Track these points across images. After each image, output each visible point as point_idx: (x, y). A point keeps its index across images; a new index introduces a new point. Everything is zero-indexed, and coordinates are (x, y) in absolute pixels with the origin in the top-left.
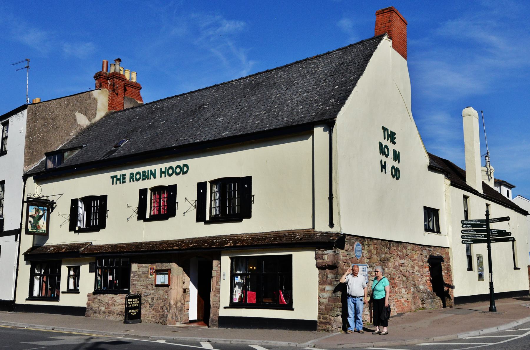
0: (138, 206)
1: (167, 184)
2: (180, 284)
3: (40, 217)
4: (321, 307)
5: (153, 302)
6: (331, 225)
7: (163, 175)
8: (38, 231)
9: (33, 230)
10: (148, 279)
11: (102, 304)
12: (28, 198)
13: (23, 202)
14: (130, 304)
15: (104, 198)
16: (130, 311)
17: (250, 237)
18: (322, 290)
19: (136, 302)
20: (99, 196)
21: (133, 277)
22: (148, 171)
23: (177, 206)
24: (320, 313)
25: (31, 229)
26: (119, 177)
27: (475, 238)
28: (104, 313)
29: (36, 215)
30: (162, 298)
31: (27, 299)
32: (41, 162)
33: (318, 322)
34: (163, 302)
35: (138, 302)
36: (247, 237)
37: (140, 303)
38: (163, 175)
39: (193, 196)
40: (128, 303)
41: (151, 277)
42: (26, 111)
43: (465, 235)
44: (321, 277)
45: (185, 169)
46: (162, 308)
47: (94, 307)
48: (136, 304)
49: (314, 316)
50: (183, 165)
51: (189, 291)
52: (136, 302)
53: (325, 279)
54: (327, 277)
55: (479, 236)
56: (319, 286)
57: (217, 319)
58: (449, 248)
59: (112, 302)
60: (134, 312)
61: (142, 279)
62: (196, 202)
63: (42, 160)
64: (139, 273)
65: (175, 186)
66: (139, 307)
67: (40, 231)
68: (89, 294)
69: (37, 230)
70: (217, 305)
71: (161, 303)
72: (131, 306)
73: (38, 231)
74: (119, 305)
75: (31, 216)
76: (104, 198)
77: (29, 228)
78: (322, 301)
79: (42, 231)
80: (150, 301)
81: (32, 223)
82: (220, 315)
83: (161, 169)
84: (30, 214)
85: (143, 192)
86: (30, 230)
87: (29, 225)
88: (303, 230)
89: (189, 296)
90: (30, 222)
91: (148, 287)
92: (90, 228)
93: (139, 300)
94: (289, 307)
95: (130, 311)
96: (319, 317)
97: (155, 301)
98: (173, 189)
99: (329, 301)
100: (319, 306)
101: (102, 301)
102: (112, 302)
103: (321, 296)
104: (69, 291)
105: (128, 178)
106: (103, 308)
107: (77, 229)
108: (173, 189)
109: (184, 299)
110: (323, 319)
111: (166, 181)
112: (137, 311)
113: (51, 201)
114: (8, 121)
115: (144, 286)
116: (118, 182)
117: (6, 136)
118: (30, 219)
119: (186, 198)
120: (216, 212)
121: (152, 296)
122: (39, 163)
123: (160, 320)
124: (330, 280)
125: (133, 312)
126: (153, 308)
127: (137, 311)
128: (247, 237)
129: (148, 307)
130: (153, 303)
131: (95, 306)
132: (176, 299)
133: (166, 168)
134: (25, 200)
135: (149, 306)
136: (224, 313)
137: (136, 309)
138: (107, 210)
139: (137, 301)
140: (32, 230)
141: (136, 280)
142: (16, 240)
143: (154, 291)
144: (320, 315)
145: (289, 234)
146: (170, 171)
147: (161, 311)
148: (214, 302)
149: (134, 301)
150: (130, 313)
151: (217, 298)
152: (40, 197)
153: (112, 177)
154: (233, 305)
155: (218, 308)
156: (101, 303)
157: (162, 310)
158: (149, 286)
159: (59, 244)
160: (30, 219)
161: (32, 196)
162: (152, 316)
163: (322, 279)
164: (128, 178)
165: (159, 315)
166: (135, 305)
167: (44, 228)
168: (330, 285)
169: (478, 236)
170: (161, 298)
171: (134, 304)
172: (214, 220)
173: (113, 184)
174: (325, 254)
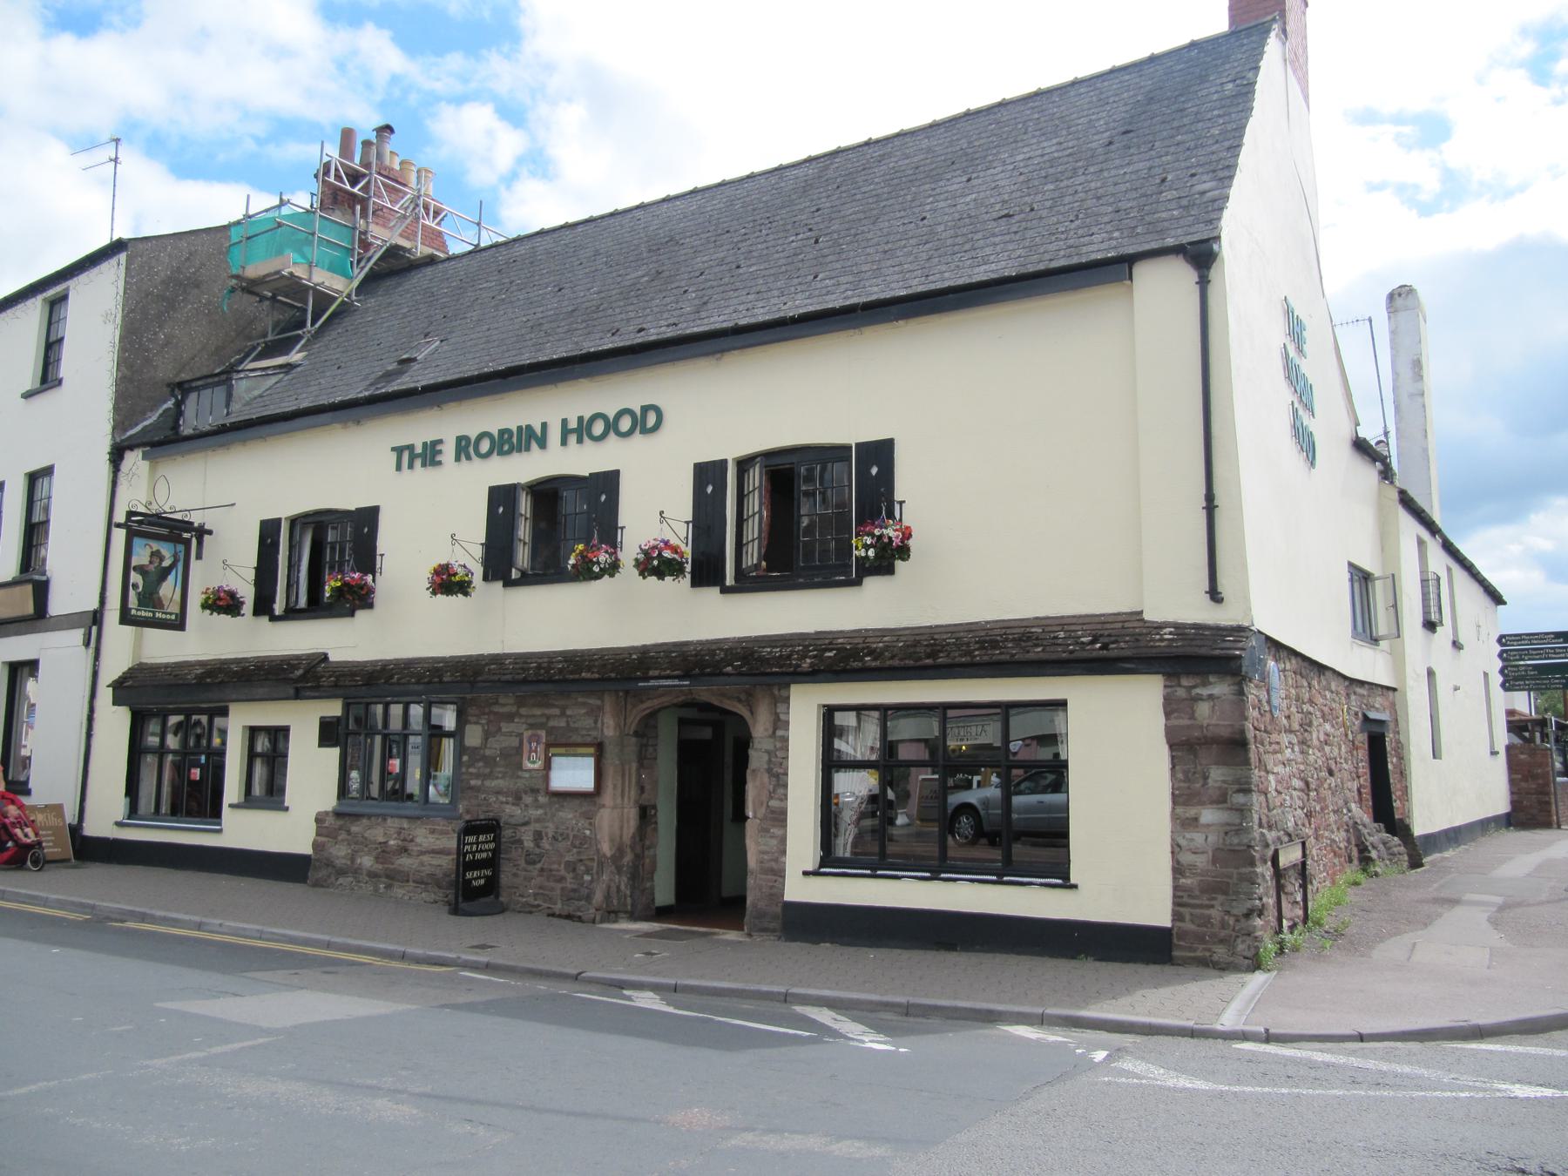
0: (484, 541)
1: (584, 471)
2: (629, 792)
3: (164, 573)
4: (1183, 881)
5: (539, 847)
6: (1215, 595)
7: (573, 439)
8: (157, 615)
9: (143, 614)
10: (520, 773)
11: (366, 849)
12: (130, 514)
13: (110, 524)
14: (471, 852)
15: (369, 517)
16: (469, 875)
17: (898, 641)
18: (1183, 823)
19: (486, 846)
20: (353, 509)
21: (469, 767)
22: (520, 428)
23: (619, 540)
24: (1178, 903)
25: (137, 610)
26: (419, 450)
27: (1545, 659)
28: (373, 875)
29: (152, 568)
30: (571, 838)
31: (119, 824)
32: (164, 411)
33: (1174, 932)
34: (575, 847)
35: (492, 846)
36: (886, 639)
37: (496, 852)
38: (573, 439)
39: (682, 508)
40: (466, 847)
41: (530, 766)
42: (123, 257)
43: (1511, 650)
44: (1180, 776)
45: (651, 419)
46: (571, 867)
47: (338, 858)
48: (486, 851)
49: (1155, 910)
50: (642, 407)
51: (655, 814)
52: (486, 846)
53: (1198, 785)
54: (1206, 778)
55: (1559, 653)
56: (1173, 809)
57: (779, 910)
58: (1394, 690)
59: (400, 843)
60: (480, 878)
61: (500, 772)
62: (691, 525)
63: (165, 406)
64: (488, 752)
65: (615, 475)
66: (493, 863)
67: (164, 616)
68: (319, 814)
69: (154, 613)
70: (773, 865)
71: (568, 852)
72: (474, 857)
73: (157, 615)
74: (422, 853)
75: (135, 569)
76: (369, 517)
77: (130, 606)
78: (1187, 858)
79: (168, 617)
80: (528, 843)
81: (140, 589)
82: (787, 898)
83: (565, 422)
84: (134, 563)
85: (501, 497)
86: (133, 612)
87: (132, 594)
88: (1114, 614)
89: (655, 830)
90: (135, 586)
91: (520, 799)
92: (316, 608)
93: (494, 841)
94: (1058, 872)
95: (469, 875)
96: (1177, 916)
97: (545, 844)
98: (608, 482)
99: (1214, 862)
100: (1175, 879)
101: (366, 839)
102: (400, 843)
103: (1183, 842)
104: (249, 801)
105: (449, 450)
106: (367, 861)
107: (515, 574)
108: (608, 482)
109: (641, 840)
110: (1192, 921)
111: (581, 461)
112: (488, 873)
113: (196, 525)
114: (67, 289)
115: (506, 794)
116: (418, 462)
117: (59, 337)
118: (135, 577)
119: (662, 513)
120: (752, 556)
121: (538, 826)
122: (157, 415)
123: (566, 907)
124: (1220, 788)
125: (477, 878)
126: (539, 866)
127: (488, 873)
128: (886, 639)
129: (523, 861)
130: (537, 851)
131: (339, 852)
132: (618, 839)
133: (580, 419)
134: (120, 517)
135: (526, 861)
136: (800, 889)
137: (486, 868)
138: (378, 553)
139: (490, 842)
140: (139, 613)
141: (477, 776)
142: (87, 644)
143: (540, 812)
144: (1182, 909)
145: (1047, 629)
146: (598, 428)
147: (569, 876)
148: (762, 856)
149: (483, 842)
150: (470, 881)
151: (774, 842)
152: (165, 513)
153: (399, 451)
154: (829, 861)
155: (780, 874)
156: (360, 843)
157: (571, 875)
158: (524, 796)
159: (223, 657)
160: (135, 577)
161: (142, 509)
162: (537, 891)
163: (1186, 785)
164: (449, 450)
165: (562, 889)
166: (484, 855)
167: (175, 608)
168: (1220, 806)
169: (1555, 653)
170: (568, 835)
171: (482, 851)
172: (747, 583)
173: (399, 468)
174: (1202, 700)
